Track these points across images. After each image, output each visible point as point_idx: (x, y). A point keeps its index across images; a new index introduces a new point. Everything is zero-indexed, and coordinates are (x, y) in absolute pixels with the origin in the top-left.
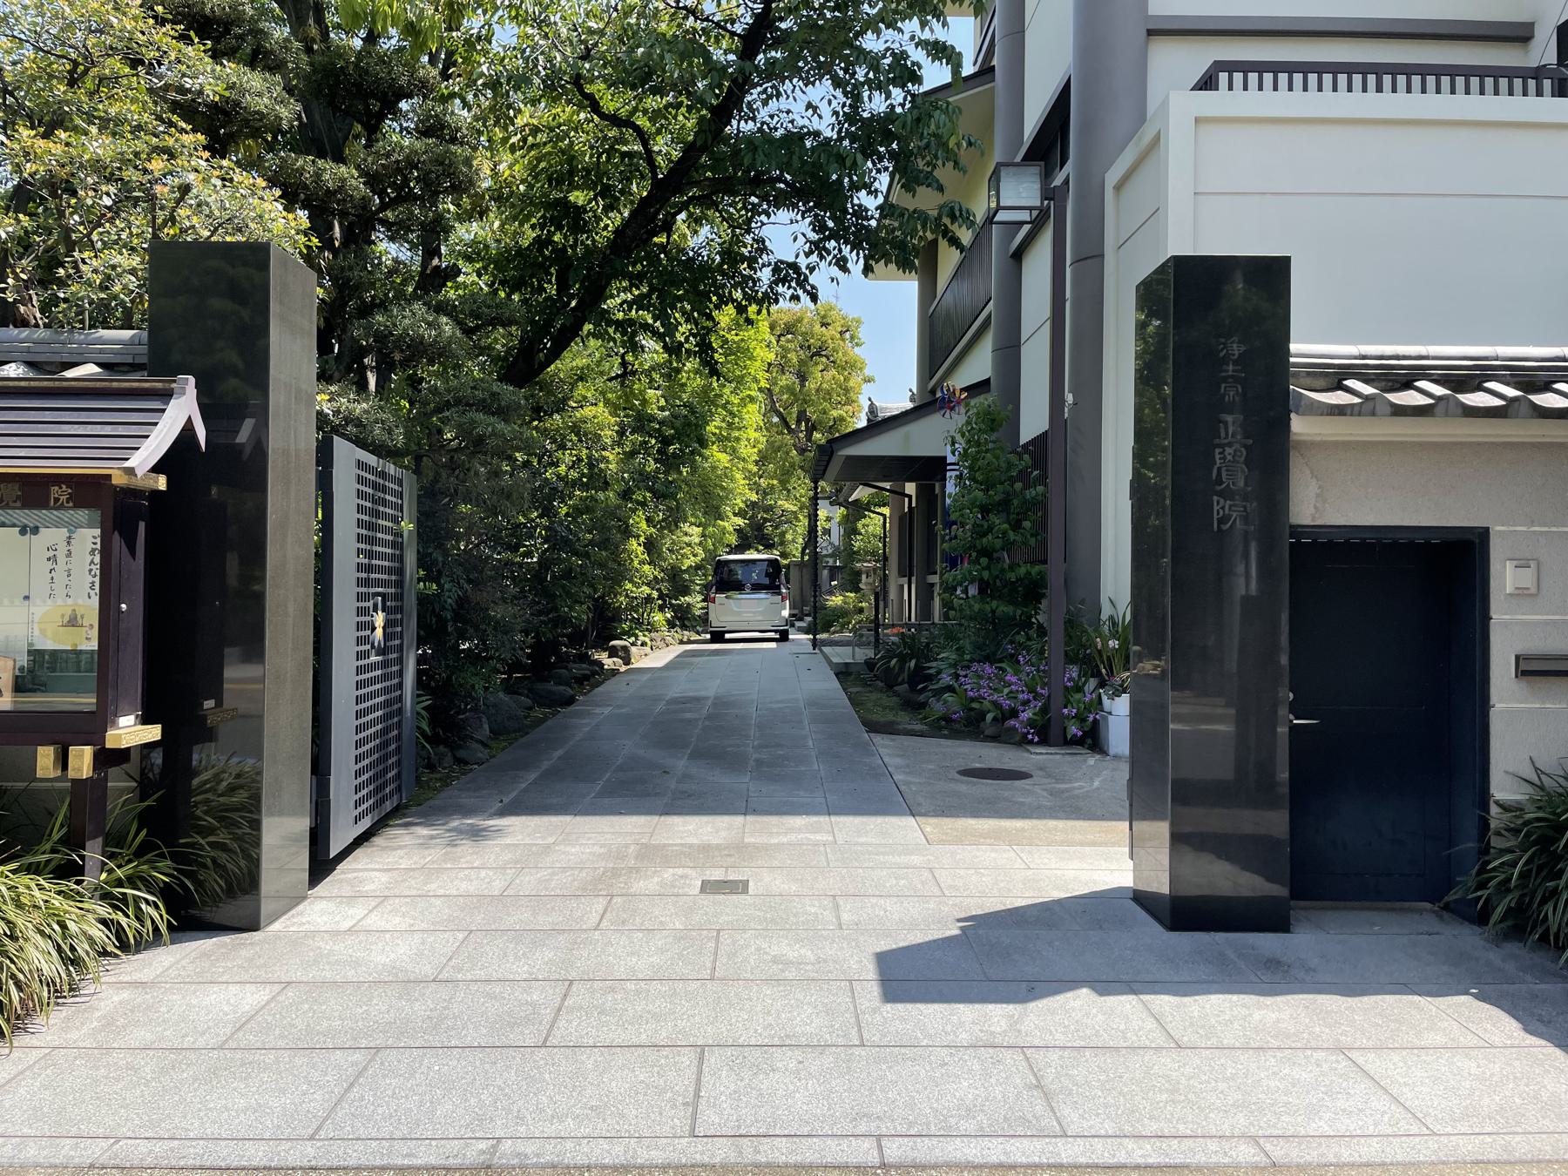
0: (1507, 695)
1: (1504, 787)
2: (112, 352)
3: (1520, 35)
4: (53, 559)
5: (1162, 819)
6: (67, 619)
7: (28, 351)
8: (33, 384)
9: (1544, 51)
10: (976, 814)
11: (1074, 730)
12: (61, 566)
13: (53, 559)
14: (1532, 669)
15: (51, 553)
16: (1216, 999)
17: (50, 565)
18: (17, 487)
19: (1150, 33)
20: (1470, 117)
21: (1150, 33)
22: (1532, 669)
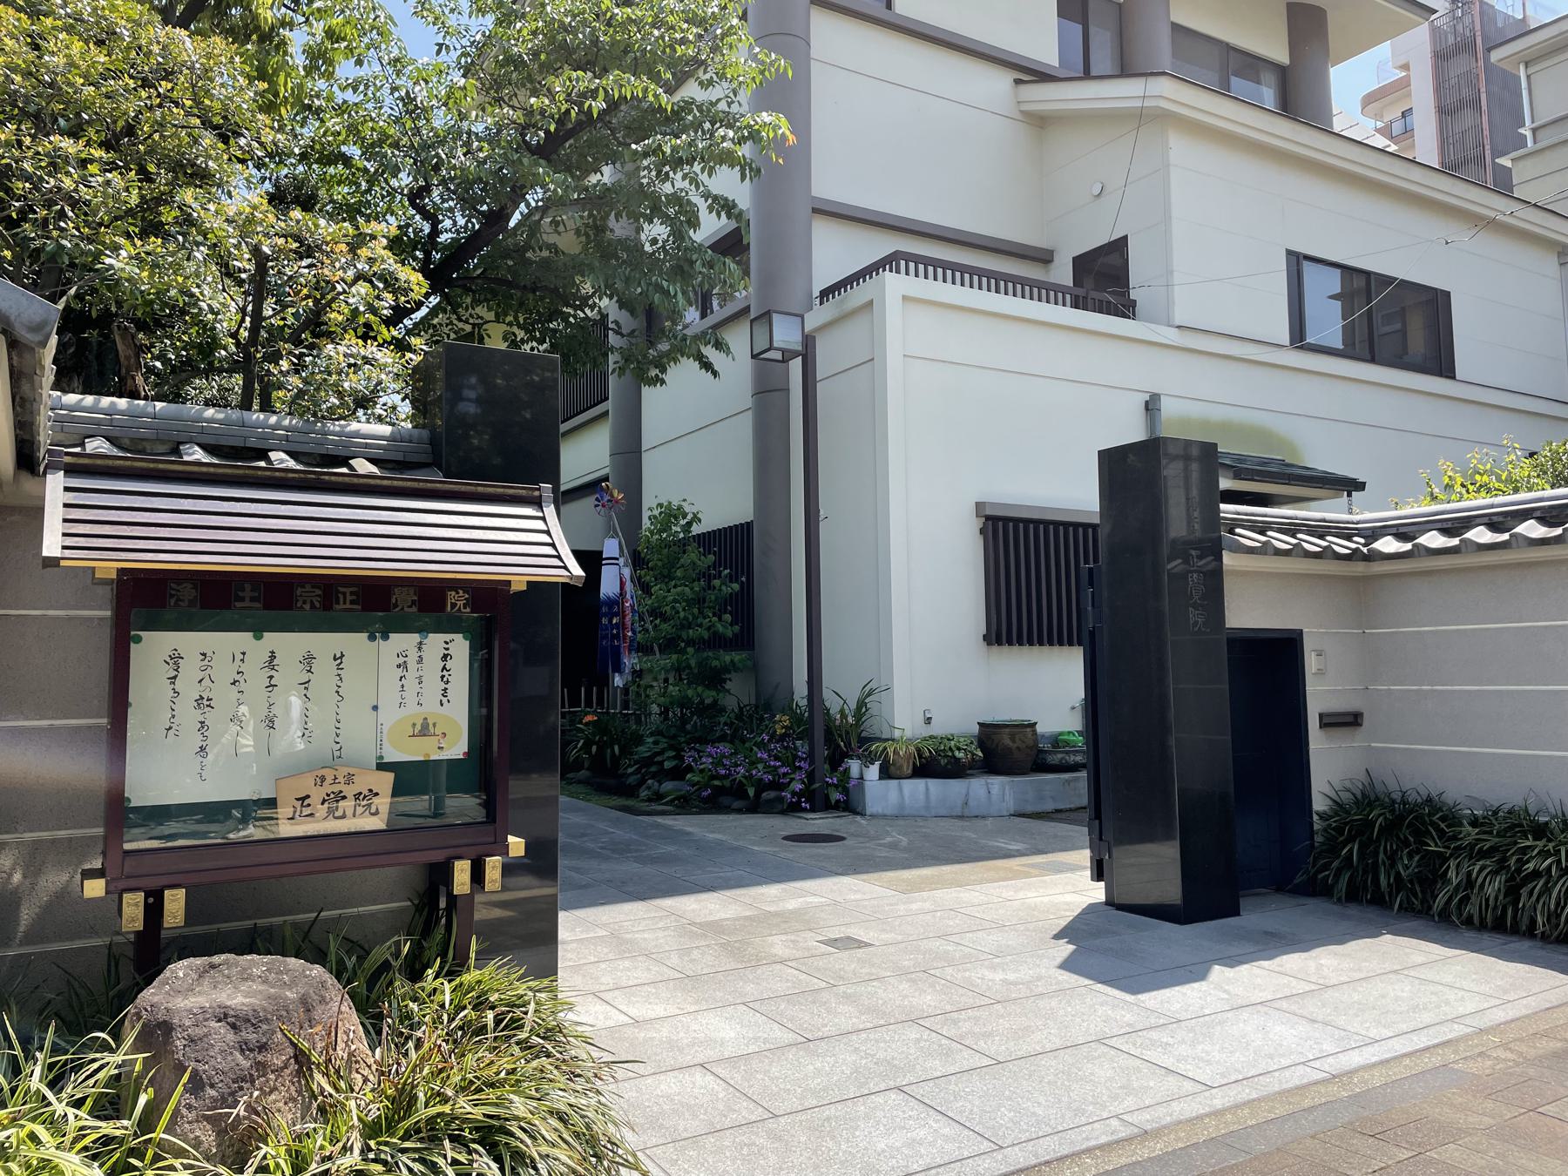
0: (1318, 741)
1: (1319, 804)
2: (379, 447)
3: (1044, 258)
4: (403, 666)
5: (1168, 837)
6: (418, 727)
7: (287, 438)
8: (128, 463)
9: (1062, 273)
10: (909, 867)
11: (836, 796)
12: (412, 674)
13: (403, 666)
14: (1331, 722)
15: (401, 660)
16: (1353, 943)
17: (400, 672)
18: (412, 591)
19: (815, 211)
20: (972, 305)
21: (815, 211)
22: (1331, 722)
